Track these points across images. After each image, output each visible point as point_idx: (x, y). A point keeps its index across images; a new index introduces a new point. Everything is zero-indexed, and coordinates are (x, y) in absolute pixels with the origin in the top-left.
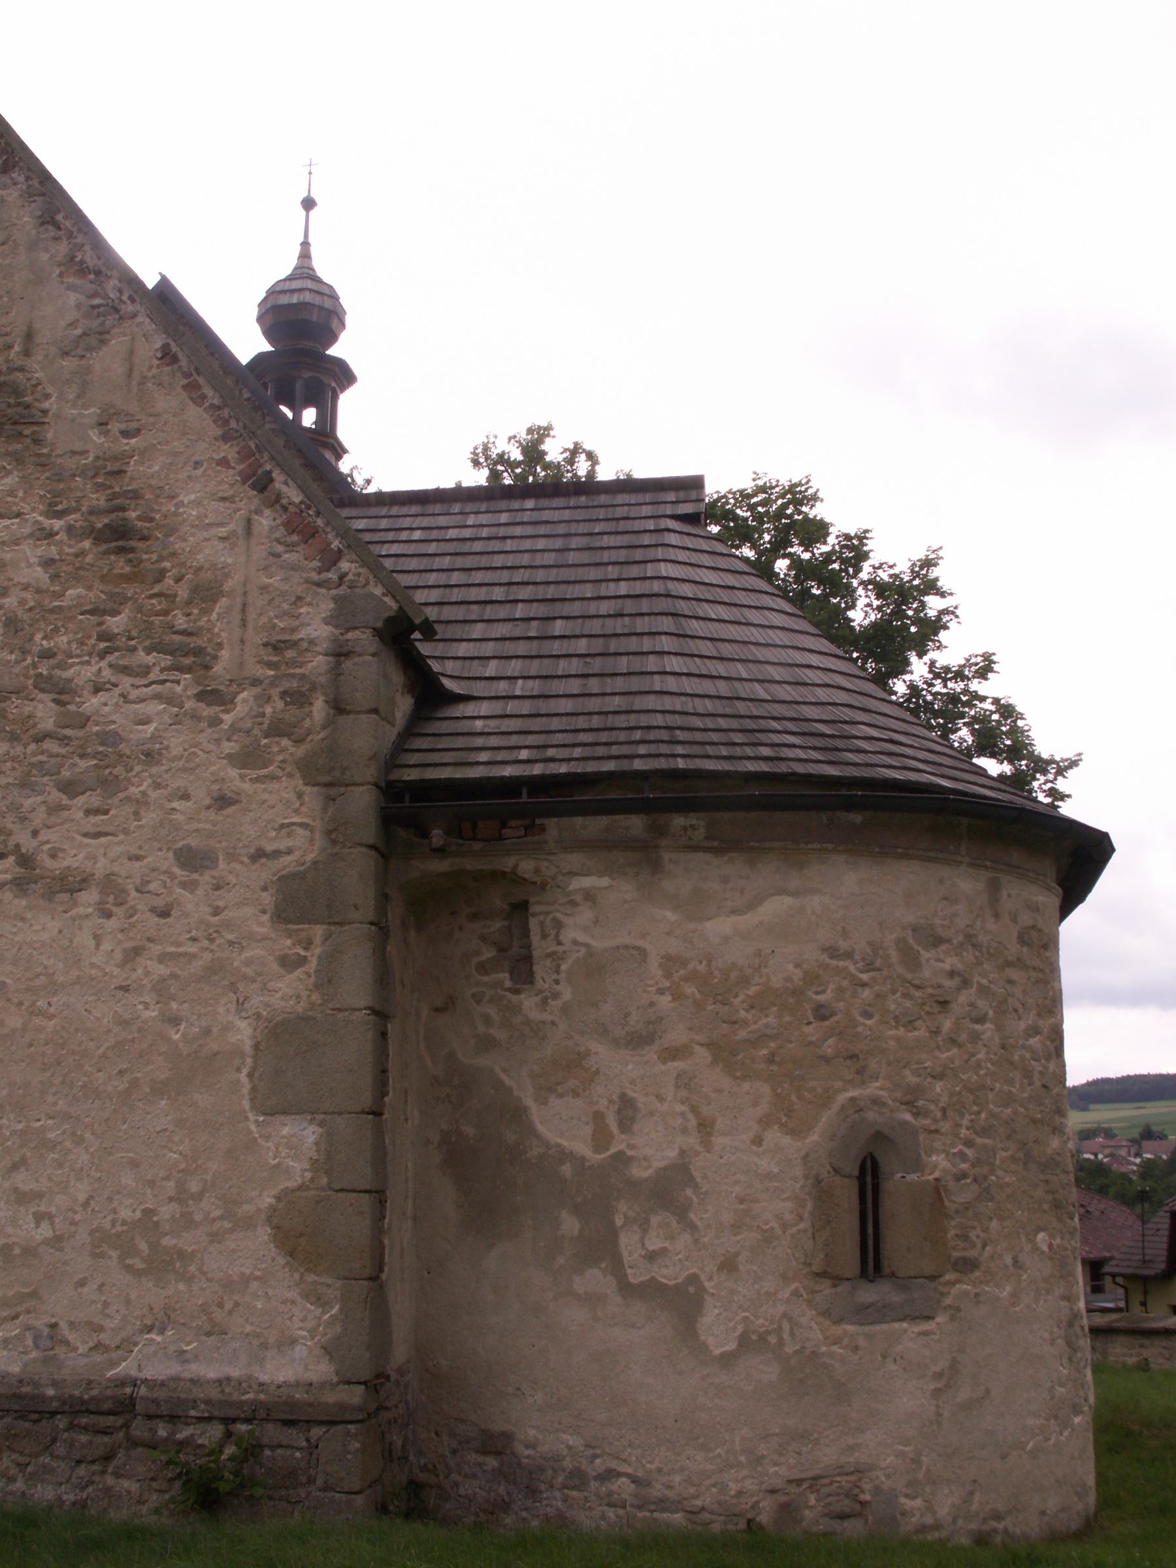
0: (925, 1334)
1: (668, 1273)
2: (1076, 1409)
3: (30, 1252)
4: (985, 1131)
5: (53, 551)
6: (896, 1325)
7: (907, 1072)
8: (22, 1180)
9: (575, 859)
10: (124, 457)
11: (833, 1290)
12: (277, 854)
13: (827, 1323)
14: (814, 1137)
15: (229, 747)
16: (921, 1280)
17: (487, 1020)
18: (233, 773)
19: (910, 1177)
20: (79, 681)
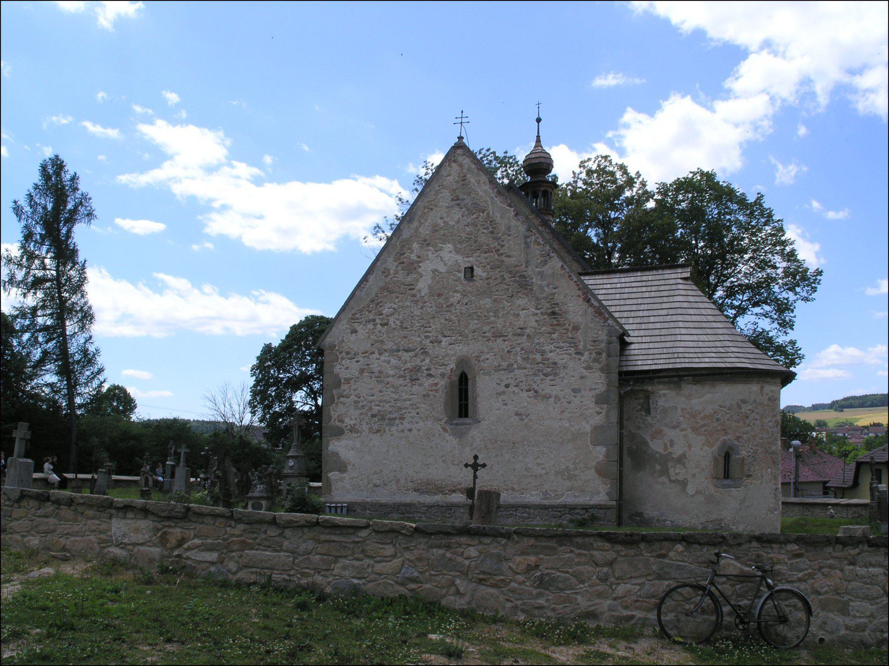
1: (680, 478)
2: (776, 510)
3: (541, 476)
4: (756, 446)
5: (538, 318)
8: (538, 461)
9: (661, 387)
10: (554, 294)
12: (595, 389)
14: (714, 448)
15: (583, 365)
17: (639, 422)
18: (585, 371)
20: (547, 350)
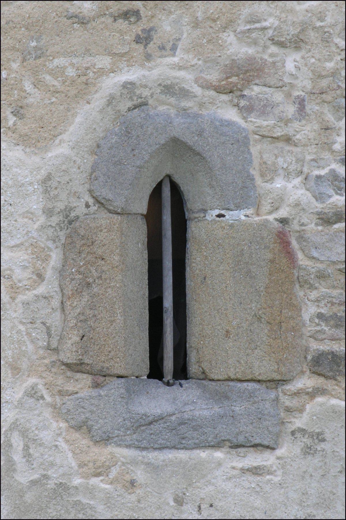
0: (256, 471)
6: (203, 454)
7: (229, 37)
11: (94, 393)
13: (85, 442)
16: (251, 386)
19: (231, 216)
